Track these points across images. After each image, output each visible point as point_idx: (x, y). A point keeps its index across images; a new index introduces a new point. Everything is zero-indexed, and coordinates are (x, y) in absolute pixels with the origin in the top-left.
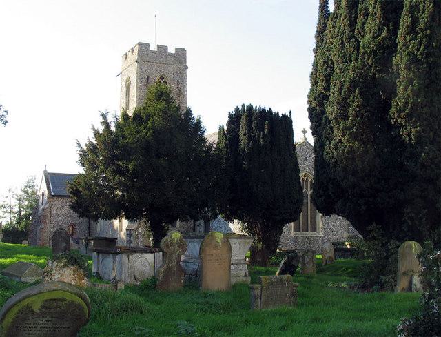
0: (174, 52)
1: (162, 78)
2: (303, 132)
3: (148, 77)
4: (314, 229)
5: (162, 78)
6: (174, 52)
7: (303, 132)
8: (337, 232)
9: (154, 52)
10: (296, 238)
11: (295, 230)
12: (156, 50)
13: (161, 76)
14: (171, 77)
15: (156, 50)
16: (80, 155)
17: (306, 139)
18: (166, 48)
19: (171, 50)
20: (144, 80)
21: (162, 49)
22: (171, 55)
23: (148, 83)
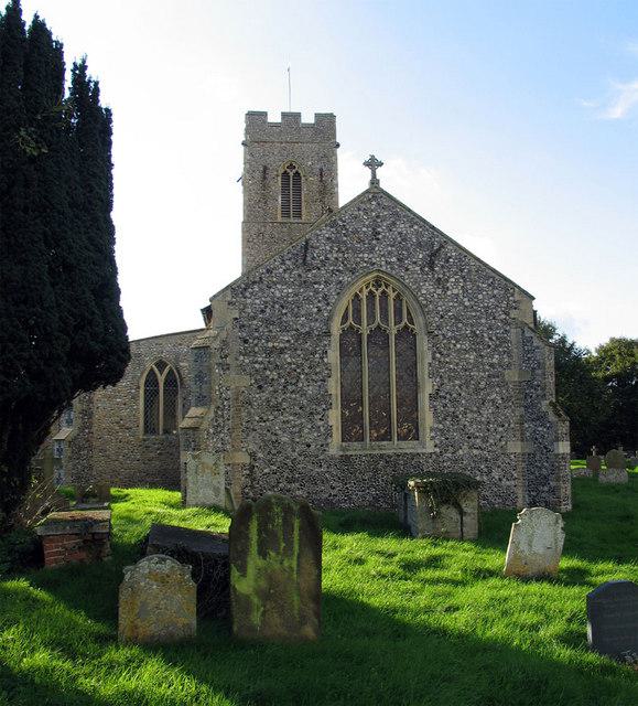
0: (278, 119)
1: (291, 167)
2: (367, 164)
3: (265, 168)
4: (414, 433)
5: (291, 167)
6: (278, 119)
7: (367, 164)
8: (485, 440)
9: (276, 125)
10: (346, 459)
11: (346, 436)
12: (280, 121)
13: (381, 164)
14: (308, 164)
15: (280, 121)
16: (549, 326)
17: (374, 182)
18: (298, 115)
19: (308, 118)
20: (258, 175)
21: (291, 118)
22: (308, 126)
23: (265, 178)
